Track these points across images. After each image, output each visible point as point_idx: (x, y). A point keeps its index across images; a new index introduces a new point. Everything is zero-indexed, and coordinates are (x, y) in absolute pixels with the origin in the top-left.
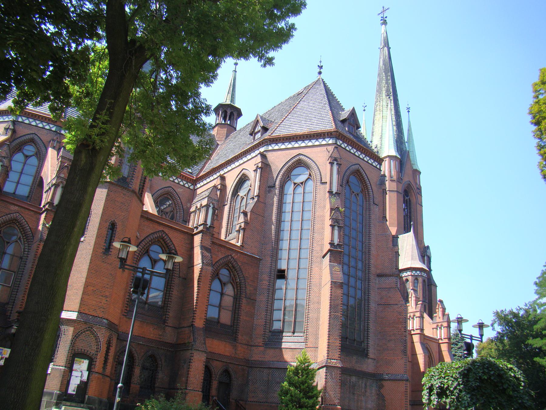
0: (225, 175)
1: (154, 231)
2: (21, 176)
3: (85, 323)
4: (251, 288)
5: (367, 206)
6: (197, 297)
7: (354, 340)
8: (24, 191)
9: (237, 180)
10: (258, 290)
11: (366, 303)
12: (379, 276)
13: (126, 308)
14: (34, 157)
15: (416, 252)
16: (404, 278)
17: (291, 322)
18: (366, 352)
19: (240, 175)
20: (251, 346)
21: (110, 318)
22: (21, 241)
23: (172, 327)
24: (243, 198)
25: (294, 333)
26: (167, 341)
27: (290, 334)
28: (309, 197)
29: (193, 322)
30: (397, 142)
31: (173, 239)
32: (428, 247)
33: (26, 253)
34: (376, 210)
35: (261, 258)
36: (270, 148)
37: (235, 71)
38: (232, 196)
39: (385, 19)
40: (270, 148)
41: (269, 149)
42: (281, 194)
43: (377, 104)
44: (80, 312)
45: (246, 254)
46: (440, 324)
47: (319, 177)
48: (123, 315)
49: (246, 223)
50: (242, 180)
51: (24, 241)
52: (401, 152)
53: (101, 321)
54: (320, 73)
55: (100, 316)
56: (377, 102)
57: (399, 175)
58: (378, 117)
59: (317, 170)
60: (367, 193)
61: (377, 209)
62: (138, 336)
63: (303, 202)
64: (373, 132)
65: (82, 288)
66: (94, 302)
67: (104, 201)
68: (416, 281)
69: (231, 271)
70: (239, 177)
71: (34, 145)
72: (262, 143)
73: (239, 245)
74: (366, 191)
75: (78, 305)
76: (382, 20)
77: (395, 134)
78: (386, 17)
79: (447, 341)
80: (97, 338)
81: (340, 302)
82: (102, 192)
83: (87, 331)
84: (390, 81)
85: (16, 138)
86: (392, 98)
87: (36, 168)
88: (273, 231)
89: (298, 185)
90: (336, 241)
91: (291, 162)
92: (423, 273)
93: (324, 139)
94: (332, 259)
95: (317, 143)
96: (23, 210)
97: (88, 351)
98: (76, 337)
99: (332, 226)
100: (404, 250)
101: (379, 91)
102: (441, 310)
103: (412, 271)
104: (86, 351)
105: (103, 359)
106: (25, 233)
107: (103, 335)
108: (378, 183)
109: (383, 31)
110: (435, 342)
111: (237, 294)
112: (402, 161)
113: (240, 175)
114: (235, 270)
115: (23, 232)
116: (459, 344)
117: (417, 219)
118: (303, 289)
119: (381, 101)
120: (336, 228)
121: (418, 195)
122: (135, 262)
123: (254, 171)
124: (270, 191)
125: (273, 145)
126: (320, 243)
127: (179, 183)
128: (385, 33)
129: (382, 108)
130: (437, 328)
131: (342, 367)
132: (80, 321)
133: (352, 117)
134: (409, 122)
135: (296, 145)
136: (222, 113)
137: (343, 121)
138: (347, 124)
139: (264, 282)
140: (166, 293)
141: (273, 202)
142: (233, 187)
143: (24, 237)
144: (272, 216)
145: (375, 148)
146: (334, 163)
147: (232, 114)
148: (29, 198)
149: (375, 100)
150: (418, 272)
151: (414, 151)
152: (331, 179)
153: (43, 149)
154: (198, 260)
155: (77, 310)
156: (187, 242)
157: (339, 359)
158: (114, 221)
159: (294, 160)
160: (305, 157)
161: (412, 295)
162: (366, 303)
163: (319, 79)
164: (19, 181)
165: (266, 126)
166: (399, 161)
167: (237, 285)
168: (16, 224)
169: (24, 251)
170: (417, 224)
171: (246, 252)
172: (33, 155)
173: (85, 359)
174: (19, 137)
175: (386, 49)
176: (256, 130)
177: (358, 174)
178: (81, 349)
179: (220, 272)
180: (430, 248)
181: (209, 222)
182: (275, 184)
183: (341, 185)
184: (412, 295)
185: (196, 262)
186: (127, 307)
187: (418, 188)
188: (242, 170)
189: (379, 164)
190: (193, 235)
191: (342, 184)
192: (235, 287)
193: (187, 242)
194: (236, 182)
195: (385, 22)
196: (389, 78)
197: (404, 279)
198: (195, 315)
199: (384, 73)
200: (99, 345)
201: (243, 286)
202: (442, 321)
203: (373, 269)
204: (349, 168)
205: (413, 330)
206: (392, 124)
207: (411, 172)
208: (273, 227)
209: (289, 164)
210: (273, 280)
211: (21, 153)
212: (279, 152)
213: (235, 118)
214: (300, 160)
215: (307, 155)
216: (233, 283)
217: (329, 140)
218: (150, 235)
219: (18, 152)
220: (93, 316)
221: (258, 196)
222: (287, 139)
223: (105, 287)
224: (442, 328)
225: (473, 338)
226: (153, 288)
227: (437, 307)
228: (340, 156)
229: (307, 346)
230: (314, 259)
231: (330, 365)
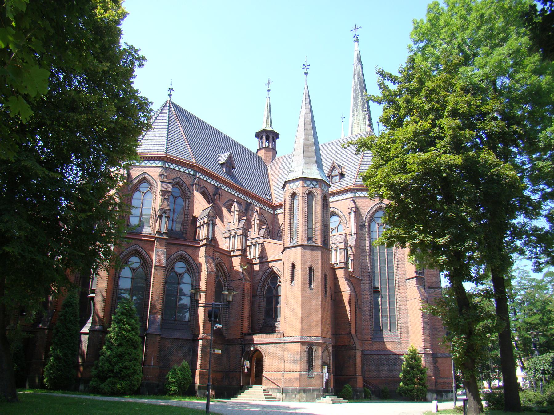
40: (357, 195)
43: (354, 117)
65: (320, 321)
78: (359, 35)
101: (356, 105)
119: (358, 116)
124: (361, 229)
129: (359, 121)
141: (365, 237)
175: (360, 66)
182: (364, 224)
185: (342, 289)
195: (357, 41)
199: (359, 90)
205: (233, 251)
208: (367, 256)
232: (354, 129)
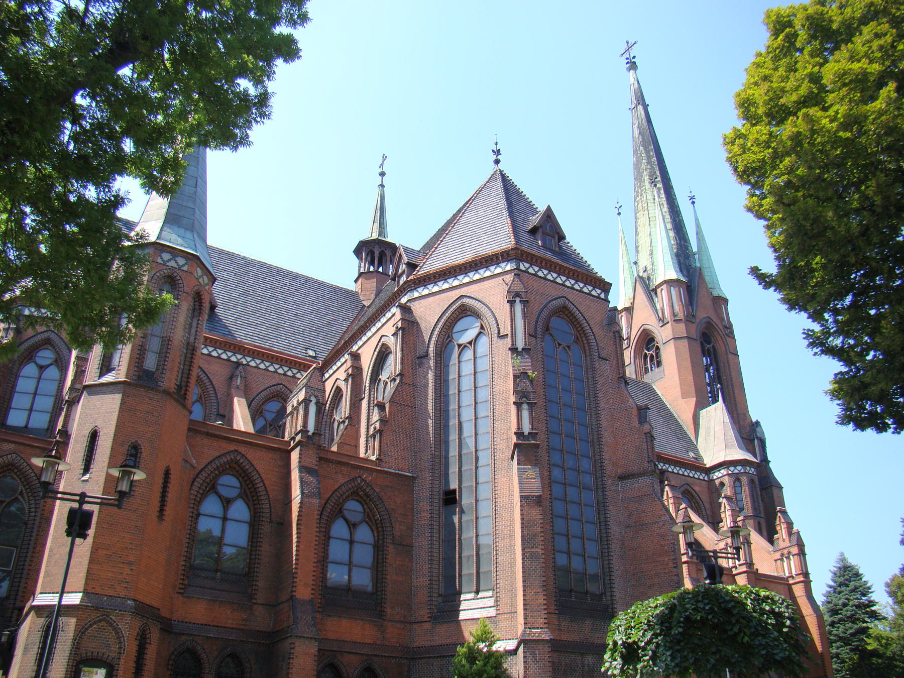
0: (359, 352)
1: (222, 452)
2: (34, 398)
3: (97, 609)
4: (402, 528)
5: (589, 363)
6: (297, 550)
7: (571, 591)
8: (40, 421)
9: (375, 356)
10: (414, 529)
11: (603, 527)
12: (623, 478)
13: (182, 582)
14: (52, 367)
15: (731, 434)
16: (716, 481)
17: (472, 574)
18: (610, 610)
19: (379, 347)
20: (411, 623)
21: (140, 598)
22: (23, 497)
23: (266, 605)
24: (387, 383)
25: (477, 592)
26: (257, 628)
27: (471, 596)
28: (483, 364)
29: (292, 592)
30: (677, 255)
31: (254, 463)
32: (757, 423)
33: (33, 514)
34: (605, 370)
35: (415, 475)
36: (416, 294)
37: (382, 186)
38: (370, 383)
39: (633, 60)
40: (416, 294)
41: (415, 296)
42: (439, 365)
43: (638, 199)
44: (86, 592)
45: (387, 472)
46: (785, 552)
47: (494, 328)
48: (177, 593)
49: (382, 420)
50: (383, 355)
51: (28, 497)
52: (688, 271)
53: (123, 604)
54: (497, 162)
55: (122, 594)
56: (636, 197)
57: (688, 310)
58: (643, 220)
59: (491, 316)
60: (585, 342)
61: (607, 367)
62: (206, 625)
63: (475, 373)
64: (637, 247)
65: (89, 553)
66: (110, 574)
67: (117, 413)
68: (737, 483)
69: (364, 504)
70: (377, 350)
71: (51, 348)
72: (404, 289)
73: (374, 459)
74: (584, 339)
75: (83, 582)
76: (628, 63)
77: (673, 242)
78: (634, 57)
79: (802, 579)
80: (117, 631)
81: (539, 529)
82: (114, 399)
83: (100, 621)
84: (655, 158)
85: (23, 340)
86: (660, 185)
87: (57, 383)
88: (431, 429)
89: (465, 346)
90: (527, 429)
91: (449, 312)
92: (748, 468)
93: (498, 264)
94: (522, 459)
95: (488, 274)
96: (21, 448)
97: (103, 654)
98: (81, 633)
99: (518, 405)
100: (712, 433)
101: (638, 178)
102: (785, 526)
103: (728, 468)
104: (100, 654)
105: (132, 664)
106: (28, 484)
107: (128, 627)
108: (604, 323)
109: (632, 80)
110: (781, 583)
111: (378, 539)
112: (690, 286)
113: (379, 347)
114: (370, 500)
115: (25, 483)
116: (851, 584)
117: (731, 378)
118: (486, 517)
119: (644, 194)
120: (525, 406)
121: (727, 338)
122: (192, 505)
123: (393, 335)
124: (420, 365)
125: (420, 290)
126: (505, 437)
127: (276, 372)
128: (636, 82)
129: (646, 204)
130: (782, 560)
131: (551, 639)
132: (87, 606)
133: (548, 222)
134: (697, 220)
135: (456, 283)
136: (367, 255)
137: (533, 231)
138: (539, 235)
139: (424, 514)
140: (251, 551)
141: (427, 380)
142: (371, 369)
143: (28, 490)
144: (427, 404)
145: (644, 272)
146: (515, 301)
147: (382, 255)
148: (49, 431)
149: (633, 194)
150: (739, 468)
151: (712, 267)
152: (512, 328)
153: (65, 351)
154: (296, 491)
155: (82, 589)
156: (280, 463)
157: (546, 625)
158: (137, 441)
159: (454, 307)
160: (471, 300)
161: (725, 507)
162: (603, 527)
163: (496, 171)
164: (32, 407)
165: (413, 261)
166: (685, 286)
167: (377, 524)
168: (13, 471)
169: (30, 512)
170: (733, 387)
171: (386, 469)
172: (51, 364)
173: (100, 667)
174: (27, 340)
175: (640, 107)
176: (400, 271)
177: (564, 312)
178: (92, 653)
179: (345, 507)
180: (762, 424)
181: (311, 427)
182: (427, 352)
183: (531, 334)
184: (725, 507)
186: (183, 580)
187: (726, 327)
188: (381, 338)
189: (603, 291)
190: (289, 452)
191: (536, 334)
192: (374, 528)
193: (280, 463)
194: (374, 359)
196: (651, 154)
197: (717, 482)
198: (295, 580)
199: (642, 148)
200: (121, 643)
201: (388, 525)
202: (789, 545)
203: (609, 468)
204: (545, 306)
206: (666, 227)
207: (708, 303)
208: (430, 422)
209: (447, 315)
210: (437, 508)
211: (33, 364)
212: (431, 299)
213: (389, 259)
214: (463, 305)
215: (473, 296)
216: (370, 523)
217: (506, 265)
218: (214, 460)
219: (27, 363)
220: (110, 596)
221: (401, 375)
222: (440, 276)
223: (126, 548)
224: (791, 557)
225: (719, 555)
226: (229, 545)
227: (778, 522)
228: (524, 287)
229: (499, 612)
230: (498, 464)
231: (530, 638)
232: (639, 221)
